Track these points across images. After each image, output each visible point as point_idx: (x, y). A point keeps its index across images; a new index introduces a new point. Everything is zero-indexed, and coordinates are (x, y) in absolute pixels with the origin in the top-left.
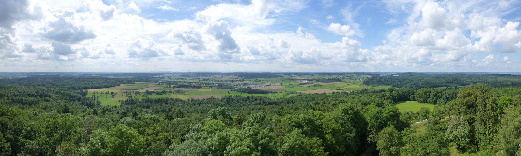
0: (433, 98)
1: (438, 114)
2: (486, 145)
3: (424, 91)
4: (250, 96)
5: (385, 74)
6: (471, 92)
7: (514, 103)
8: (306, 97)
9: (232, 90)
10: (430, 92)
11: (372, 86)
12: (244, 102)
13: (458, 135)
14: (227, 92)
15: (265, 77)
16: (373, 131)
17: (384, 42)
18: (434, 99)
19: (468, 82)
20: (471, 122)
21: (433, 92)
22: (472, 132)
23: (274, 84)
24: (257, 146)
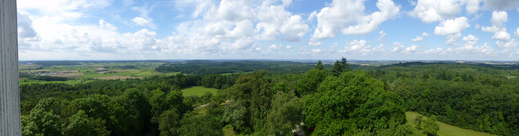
0: (218, 83)
2: (260, 127)
3: (210, 77)
4: (48, 84)
5: (175, 62)
6: (248, 78)
7: (287, 88)
8: (102, 83)
9: (29, 78)
10: (215, 78)
11: (163, 73)
12: (42, 90)
13: (233, 118)
14: (23, 81)
15: (64, 65)
16: (156, 114)
17: (174, 33)
20: (248, 105)
21: (218, 77)
22: (248, 114)
23: (72, 72)
24: (41, 128)
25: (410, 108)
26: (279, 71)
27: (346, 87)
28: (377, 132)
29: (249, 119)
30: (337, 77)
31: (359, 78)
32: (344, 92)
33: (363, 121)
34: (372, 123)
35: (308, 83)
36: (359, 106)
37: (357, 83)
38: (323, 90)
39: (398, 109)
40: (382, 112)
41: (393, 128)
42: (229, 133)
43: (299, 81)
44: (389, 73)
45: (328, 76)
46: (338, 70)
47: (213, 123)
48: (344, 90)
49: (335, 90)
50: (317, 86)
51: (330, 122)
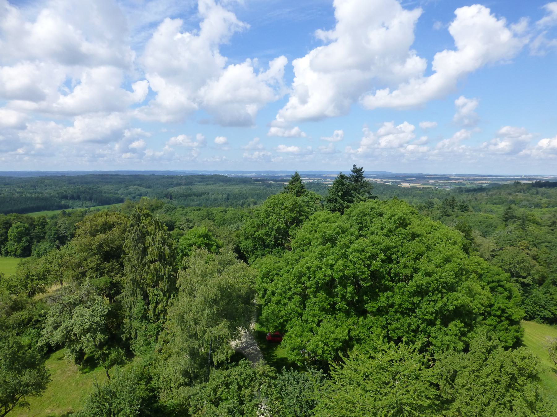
1: (24, 283)
2: (149, 344)
6: (112, 219)
7: (216, 242)
13: (75, 331)
18: (23, 244)
19: (122, 194)
21: (18, 224)
25: (537, 313)
26: (193, 201)
27: (361, 240)
28: (436, 356)
29: (120, 325)
30: (339, 213)
31: (393, 218)
32: (355, 251)
33: (402, 326)
34: (426, 332)
35: (267, 229)
36: (392, 287)
37: (390, 231)
38: (304, 245)
39: (499, 308)
40: (451, 308)
41: (480, 354)
42: (63, 372)
43: (245, 226)
44: (480, 210)
45: (316, 210)
46: (343, 197)
47: (14, 354)
48: (355, 246)
49: (334, 243)
50: (289, 236)
51: (320, 321)
